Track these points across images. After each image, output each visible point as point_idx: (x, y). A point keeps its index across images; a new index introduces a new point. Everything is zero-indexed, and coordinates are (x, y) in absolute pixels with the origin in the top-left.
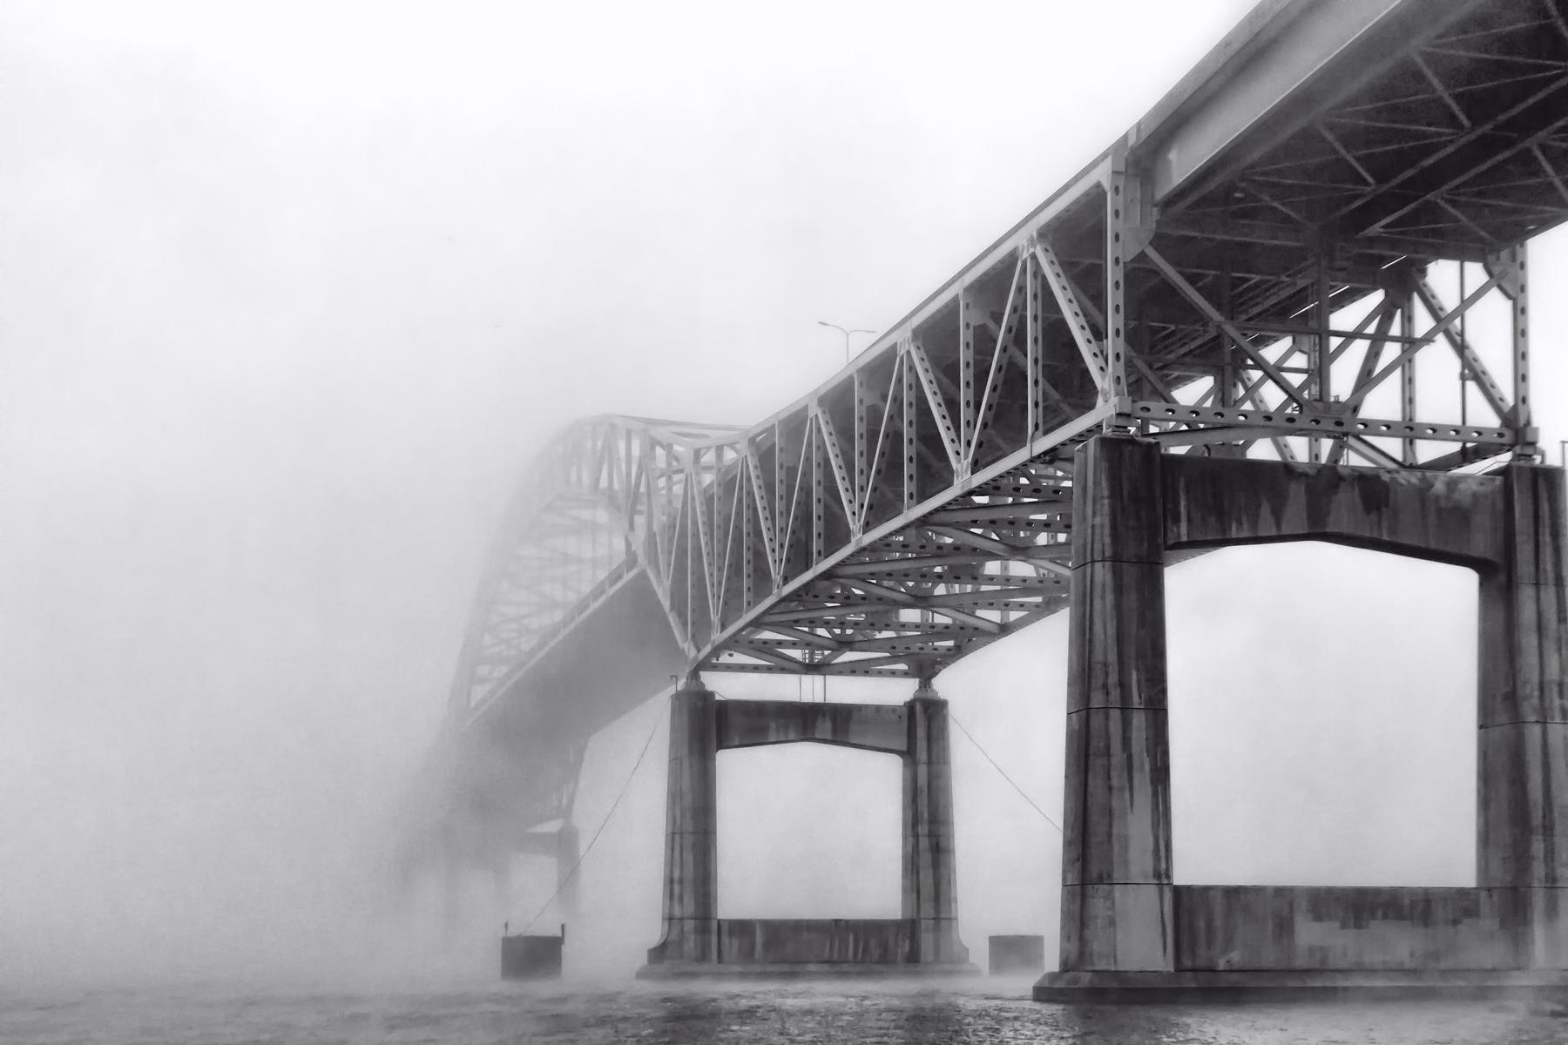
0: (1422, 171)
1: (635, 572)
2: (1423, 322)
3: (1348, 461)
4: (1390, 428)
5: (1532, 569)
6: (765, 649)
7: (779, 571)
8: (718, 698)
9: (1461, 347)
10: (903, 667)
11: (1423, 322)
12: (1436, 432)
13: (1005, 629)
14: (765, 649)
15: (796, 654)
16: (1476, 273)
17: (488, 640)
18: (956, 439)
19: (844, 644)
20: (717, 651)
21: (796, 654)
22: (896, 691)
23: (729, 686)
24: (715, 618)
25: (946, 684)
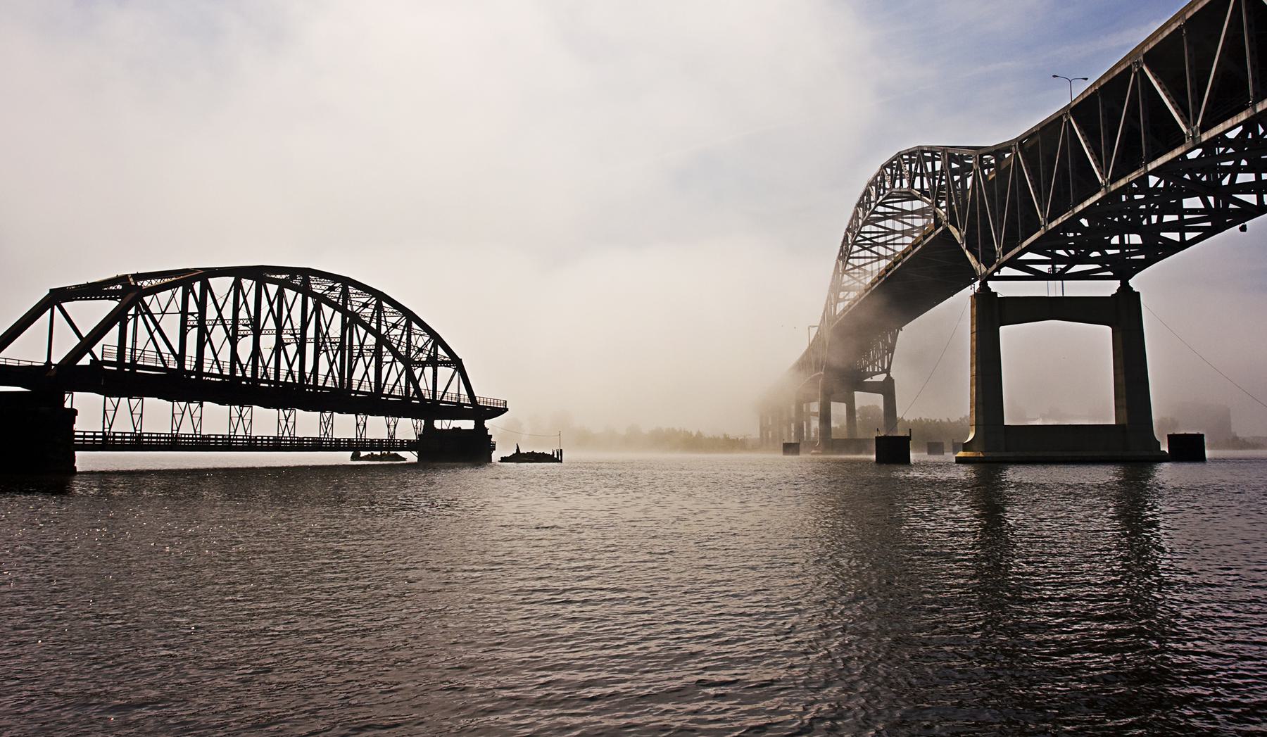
1: (941, 229)
6: (1022, 266)
8: (999, 296)
13: (1184, 244)
15: (1045, 268)
19: (1071, 261)
20: (998, 270)
22: (1109, 288)
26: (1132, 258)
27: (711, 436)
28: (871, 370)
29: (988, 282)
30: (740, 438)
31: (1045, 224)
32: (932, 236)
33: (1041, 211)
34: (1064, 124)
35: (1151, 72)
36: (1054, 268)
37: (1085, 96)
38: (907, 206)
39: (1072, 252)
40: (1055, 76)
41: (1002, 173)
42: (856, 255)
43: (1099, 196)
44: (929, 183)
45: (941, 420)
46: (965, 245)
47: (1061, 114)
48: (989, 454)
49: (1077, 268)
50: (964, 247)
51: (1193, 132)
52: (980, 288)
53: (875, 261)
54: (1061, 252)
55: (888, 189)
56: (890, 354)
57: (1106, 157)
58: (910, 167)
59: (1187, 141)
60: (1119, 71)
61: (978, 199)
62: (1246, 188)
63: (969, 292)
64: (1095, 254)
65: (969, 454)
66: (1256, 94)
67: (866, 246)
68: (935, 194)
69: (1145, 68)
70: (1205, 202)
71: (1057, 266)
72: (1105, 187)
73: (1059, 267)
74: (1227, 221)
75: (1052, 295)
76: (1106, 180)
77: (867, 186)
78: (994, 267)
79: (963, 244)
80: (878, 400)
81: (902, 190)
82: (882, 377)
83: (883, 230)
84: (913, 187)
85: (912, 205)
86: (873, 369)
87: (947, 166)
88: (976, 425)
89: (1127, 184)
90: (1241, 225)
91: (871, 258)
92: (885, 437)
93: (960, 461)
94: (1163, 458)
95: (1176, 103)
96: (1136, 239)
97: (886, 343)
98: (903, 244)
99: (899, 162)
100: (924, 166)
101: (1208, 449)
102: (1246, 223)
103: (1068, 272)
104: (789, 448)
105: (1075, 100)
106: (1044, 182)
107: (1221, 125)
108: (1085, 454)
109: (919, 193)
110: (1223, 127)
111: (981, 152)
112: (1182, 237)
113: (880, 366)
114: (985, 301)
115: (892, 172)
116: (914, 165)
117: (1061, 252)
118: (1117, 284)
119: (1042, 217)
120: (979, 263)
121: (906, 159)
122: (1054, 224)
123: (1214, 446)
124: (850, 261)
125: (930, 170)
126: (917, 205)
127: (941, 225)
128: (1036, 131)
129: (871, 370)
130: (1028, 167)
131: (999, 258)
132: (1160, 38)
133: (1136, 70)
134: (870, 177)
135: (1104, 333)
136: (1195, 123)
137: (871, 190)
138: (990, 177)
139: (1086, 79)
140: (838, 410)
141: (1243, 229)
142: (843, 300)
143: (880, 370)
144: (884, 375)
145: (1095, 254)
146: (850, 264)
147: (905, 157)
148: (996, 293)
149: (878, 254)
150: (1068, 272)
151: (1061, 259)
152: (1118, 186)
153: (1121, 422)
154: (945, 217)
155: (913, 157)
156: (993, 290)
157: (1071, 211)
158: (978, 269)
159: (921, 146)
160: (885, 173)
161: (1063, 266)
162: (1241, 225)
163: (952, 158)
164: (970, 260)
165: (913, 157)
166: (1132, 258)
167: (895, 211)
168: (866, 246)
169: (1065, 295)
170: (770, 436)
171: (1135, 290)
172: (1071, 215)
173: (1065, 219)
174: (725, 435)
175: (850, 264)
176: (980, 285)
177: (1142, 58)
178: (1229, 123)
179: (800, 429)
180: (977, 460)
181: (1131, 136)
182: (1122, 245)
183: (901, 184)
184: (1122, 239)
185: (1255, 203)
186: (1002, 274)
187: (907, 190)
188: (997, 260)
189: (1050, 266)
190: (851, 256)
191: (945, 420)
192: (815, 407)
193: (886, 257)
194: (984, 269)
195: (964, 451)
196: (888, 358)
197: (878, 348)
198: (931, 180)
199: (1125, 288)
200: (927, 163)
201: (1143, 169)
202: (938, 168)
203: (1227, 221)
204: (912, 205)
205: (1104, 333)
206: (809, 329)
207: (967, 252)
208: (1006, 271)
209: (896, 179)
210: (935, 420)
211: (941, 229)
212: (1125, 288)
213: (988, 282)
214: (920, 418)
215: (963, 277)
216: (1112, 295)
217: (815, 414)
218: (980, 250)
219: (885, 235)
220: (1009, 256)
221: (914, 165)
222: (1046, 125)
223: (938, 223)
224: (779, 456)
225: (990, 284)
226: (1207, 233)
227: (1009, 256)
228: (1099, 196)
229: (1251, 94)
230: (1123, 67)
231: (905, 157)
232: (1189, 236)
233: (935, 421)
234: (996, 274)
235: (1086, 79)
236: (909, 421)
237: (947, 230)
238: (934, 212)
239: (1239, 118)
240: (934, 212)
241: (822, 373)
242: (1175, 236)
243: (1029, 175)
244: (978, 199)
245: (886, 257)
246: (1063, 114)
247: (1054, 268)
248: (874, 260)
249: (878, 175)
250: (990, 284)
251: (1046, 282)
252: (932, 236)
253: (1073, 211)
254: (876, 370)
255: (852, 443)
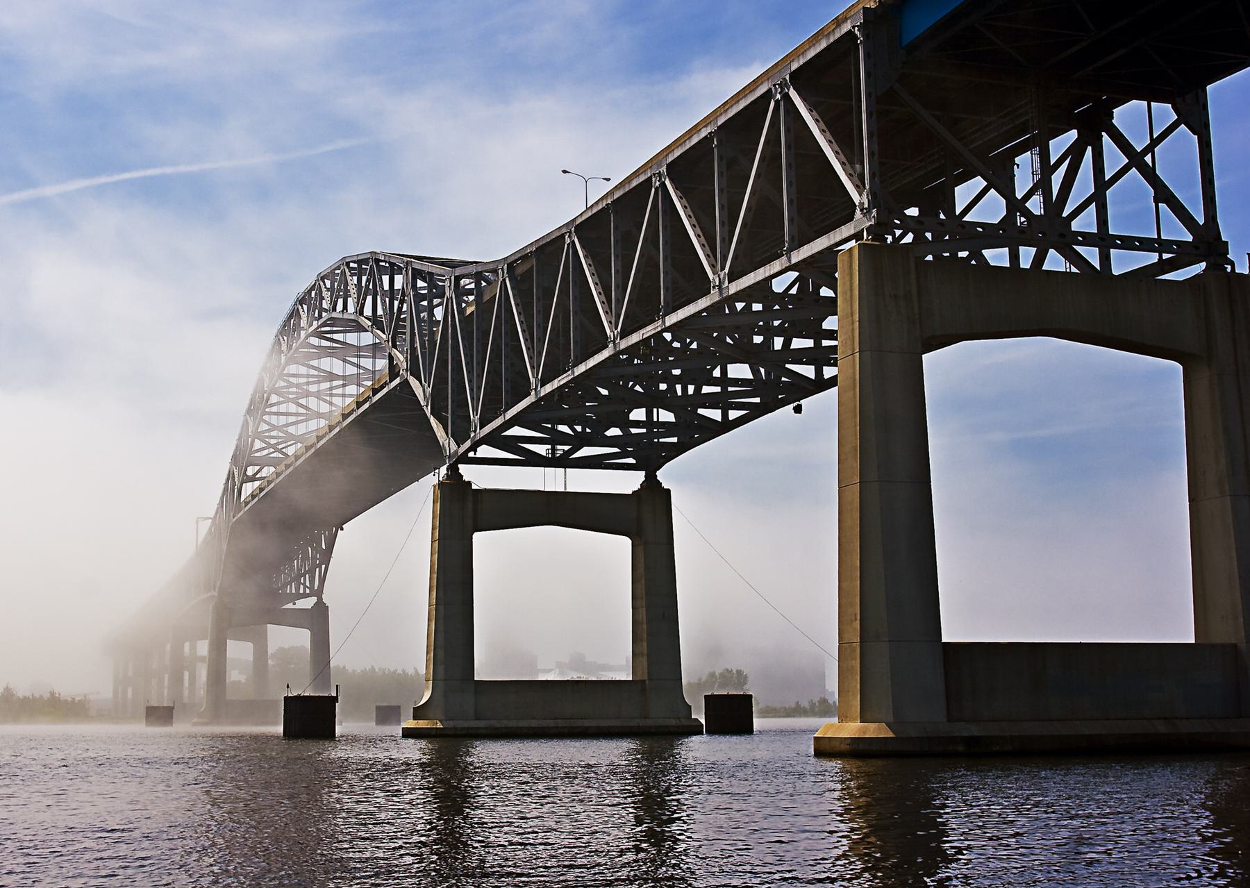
0: (296, 468)
1: (397, 381)
2: (1114, 159)
3: (565, 472)
4: (1088, 239)
5: (431, 614)
6: (511, 444)
7: (538, 375)
8: (474, 487)
9: (1150, 174)
10: (631, 461)
11: (1114, 159)
12: (1128, 243)
13: (726, 426)
14: (511, 444)
15: (541, 449)
16: (1165, 112)
17: (258, 444)
18: (609, 311)
19: (579, 441)
20: (474, 448)
21: (541, 449)
22: (627, 482)
23: (478, 477)
24: (475, 419)
25: (665, 475)
26: (661, 440)
27: (28, 694)
28: (294, 591)
29: (460, 466)
30: (77, 699)
31: (536, 387)
32: (385, 390)
33: (532, 367)
34: (566, 246)
35: (676, 188)
36: (554, 450)
37: (617, 195)
38: (351, 338)
39: (579, 428)
40: (565, 172)
41: (484, 307)
42: (274, 409)
43: (703, 303)
44: (383, 304)
45: (404, 671)
46: (429, 407)
47: (564, 231)
48: (451, 724)
49: (586, 452)
50: (428, 411)
51: (720, 279)
52: (447, 474)
53: (302, 421)
54: (564, 428)
55: (326, 311)
56: (323, 566)
57: (722, 240)
58: (360, 280)
59: (712, 292)
60: (638, 183)
61: (450, 342)
62: (802, 356)
63: (430, 481)
64: (614, 432)
65: (422, 724)
66: (792, 238)
67: (291, 396)
68: (392, 325)
69: (668, 183)
70: (755, 371)
71: (559, 447)
72: (614, 342)
73: (562, 448)
74: (780, 397)
75: (550, 488)
76: (616, 332)
77: (295, 304)
78: (468, 444)
79: (427, 406)
80: (301, 638)
81: (346, 316)
82: (309, 603)
83: (316, 373)
84: (361, 313)
85: (359, 339)
86: (298, 589)
87: (410, 287)
88: (433, 680)
89: (640, 341)
90: (796, 404)
91: (296, 414)
92: (298, 698)
93: (408, 733)
94: (696, 730)
95: (702, 237)
96: (666, 416)
97: (317, 549)
98: (344, 396)
99: (343, 273)
100: (377, 283)
101: (758, 717)
102: (803, 402)
103: (573, 456)
104: (160, 714)
105: (592, 206)
106: (722, 224)
107: (761, 270)
108: (586, 723)
109: (370, 324)
110: (755, 277)
111: (458, 271)
112: (725, 415)
113: (308, 584)
114: (454, 490)
115: (332, 284)
116: (364, 279)
117: (564, 428)
118: (638, 478)
119: (533, 377)
120: (448, 437)
121: (353, 269)
122: (549, 388)
123: (768, 712)
124: (266, 418)
125: (386, 287)
126: (367, 339)
127: (398, 375)
128: (531, 252)
129: (294, 591)
130: (519, 301)
131: (475, 431)
132: (688, 145)
133: (658, 183)
134: (302, 288)
135: (621, 546)
136: (723, 269)
137: (301, 310)
138: (469, 311)
139: (608, 180)
140: (239, 651)
141: (798, 410)
142: (253, 479)
143: (308, 591)
144: (314, 600)
145: (614, 432)
146: (265, 422)
147: (352, 265)
148: (469, 483)
149: (307, 408)
150: (573, 456)
151: (564, 439)
152: (630, 344)
153: (1224, 633)
154: (405, 364)
155: (363, 266)
156: (466, 478)
157: (570, 372)
158: (447, 446)
159: (375, 253)
160: (323, 287)
161: (567, 448)
162: (796, 404)
163: (417, 274)
164: (436, 430)
165: (363, 266)
166: (661, 440)
167: (335, 345)
168: (291, 396)
169: (567, 490)
170: (130, 695)
171: (665, 486)
172: (570, 378)
173: (562, 383)
174: (52, 694)
175: (265, 422)
176: (447, 469)
177: (664, 169)
178: (776, 266)
179: (177, 680)
180: (434, 732)
181: (765, 211)
182: (649, 423)
183: (345, 307)
184: (649, 414)
185: (813, 377)
186: (478, 455)
187: (353, 317)
188: (472, 435)
189: (549, 447)
190: (267, 410)
191: (400, 671)
192: (203, 648)
193: (319, 415)
194: (454, 447)
195: (415, 718)
196: (320, 572)
197: (305, 558)
198: (387, 299)
199: (651, 483)
200: (383, 277)
201: (660, 322)
202: (398, 284)
203: (780, 397)
204: (359, 339)
205: (621, 546)
206: (197, 522)
207: (432, 420)
208: (484, 451)
209: (337, 298)
210: (396, 670)
211: (397, 381)
212: (651, 483)
213: (460, 466)
214: (373, 667)
215: (431, 455)
216: (634, 492)
217: (202, 659)
218: (449, 416)
219: (319, 382)
220: (488, 429)
221: (364, 279)
222: (553, 240)
223: (393, 371)
224: (141, 728)
225: (463, 469)
226: (755, 412)
227: (488, 429)
228: (703, 303)
229: (787, 238)
230: (642, 178)
231: (352, 265)
232: (733, 414)
233: (395, 672)
234: (471, 454)
235: (608, 180)
236: (354, 671)
237: (405, 383)
238: (390, 354)
239: (772, 268)
240: (390, 354)
241: (216, 594)
242: (715, 414)
243: (519, 314)
244: (450, 342)
245: (319, 415)
246: (566, 233)
247: (554, 450)
248: (300, 418)
249: (313, 288)
250: (463, 469)
251: (553, 469)
252: (385, 390)
253: (573, 373)
254: (301, 591)
255: (253, 708)
